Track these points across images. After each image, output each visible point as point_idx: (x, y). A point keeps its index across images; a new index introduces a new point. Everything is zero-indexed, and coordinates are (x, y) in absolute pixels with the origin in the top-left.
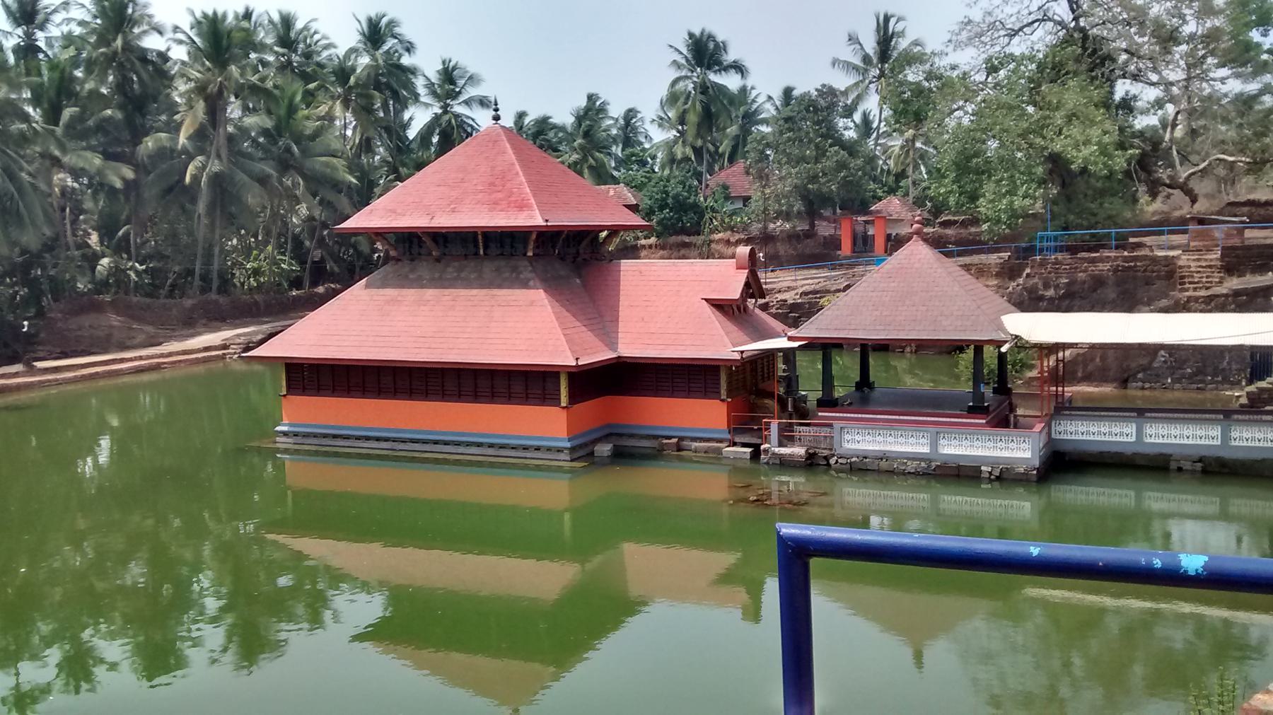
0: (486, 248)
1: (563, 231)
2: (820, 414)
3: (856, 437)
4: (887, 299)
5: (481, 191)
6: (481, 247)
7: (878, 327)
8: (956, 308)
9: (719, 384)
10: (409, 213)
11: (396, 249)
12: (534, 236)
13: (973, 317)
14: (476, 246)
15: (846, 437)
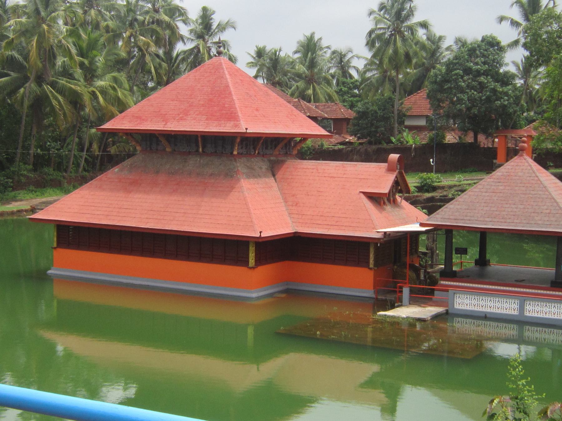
0: (204, 147)
1: (263, 137)
2: (442, 282)
3: (481, 303)
4: (495, 198)
5: (203, 105)
6: (200, 146)
7: (487, 219)
8: (545, 207)
9: (369, 256)
10: (149, 120)
11: (140, 145)
12: (238, 140)
13: (557, 215)
14: (197, 146)
15: (458, 300)
